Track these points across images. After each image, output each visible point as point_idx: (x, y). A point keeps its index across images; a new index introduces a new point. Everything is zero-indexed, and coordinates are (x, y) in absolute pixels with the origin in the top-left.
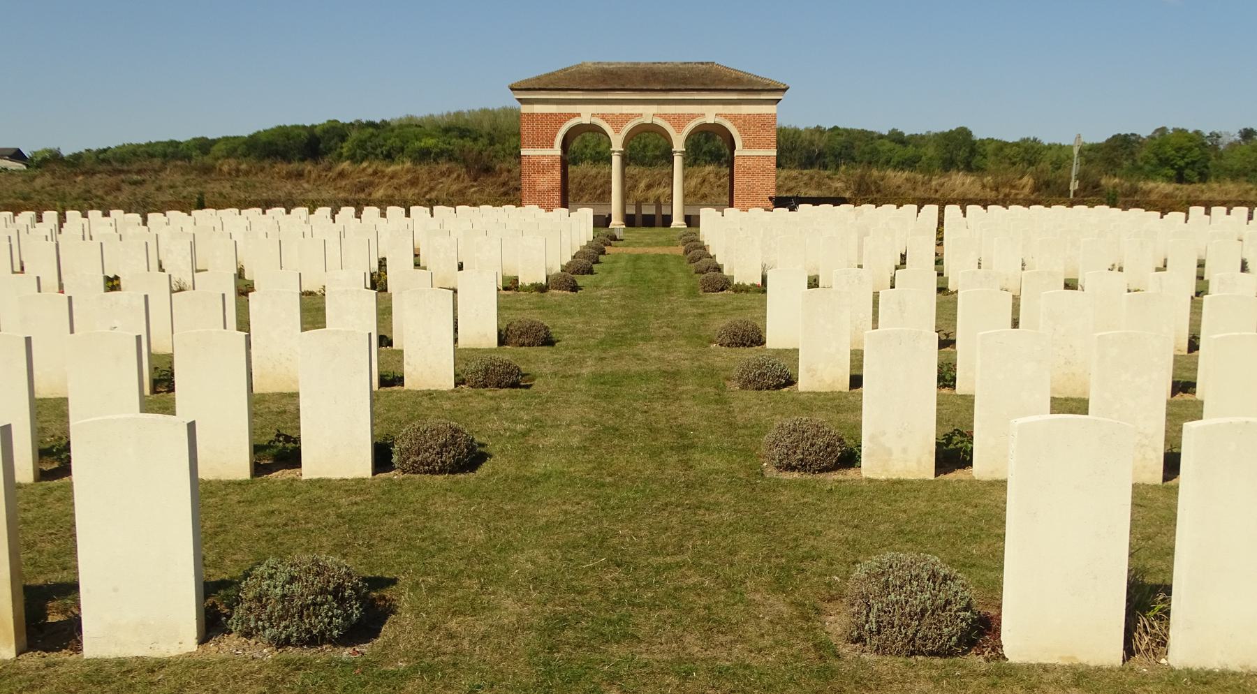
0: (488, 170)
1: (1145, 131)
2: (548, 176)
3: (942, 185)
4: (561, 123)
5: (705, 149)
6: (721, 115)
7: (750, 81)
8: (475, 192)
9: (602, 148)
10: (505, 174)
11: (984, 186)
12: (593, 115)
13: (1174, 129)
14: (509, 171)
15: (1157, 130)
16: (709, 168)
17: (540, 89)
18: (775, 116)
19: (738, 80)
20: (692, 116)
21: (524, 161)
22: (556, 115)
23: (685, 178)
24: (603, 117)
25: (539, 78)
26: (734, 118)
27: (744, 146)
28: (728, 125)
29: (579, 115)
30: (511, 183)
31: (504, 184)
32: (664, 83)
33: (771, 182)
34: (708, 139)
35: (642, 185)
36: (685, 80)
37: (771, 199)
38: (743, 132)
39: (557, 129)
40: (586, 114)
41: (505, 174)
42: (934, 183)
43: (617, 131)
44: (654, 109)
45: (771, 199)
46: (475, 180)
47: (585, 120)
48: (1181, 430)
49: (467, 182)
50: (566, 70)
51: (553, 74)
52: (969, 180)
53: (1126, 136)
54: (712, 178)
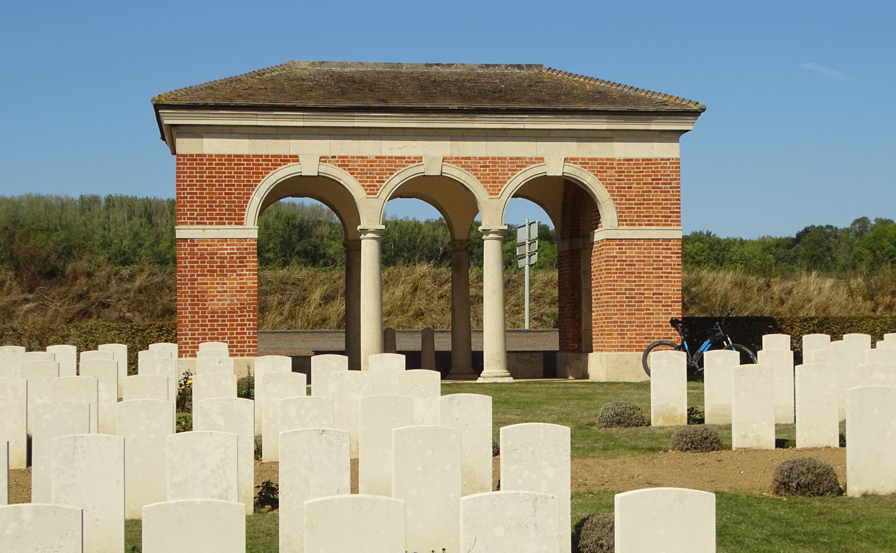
0: (52, 274)
1: (843, 221)
2: (233, 282)
3: (790, 292)
4: (259, 175)
5: (298, 248)
6: (574, 160)
7: (625, 98)
8: (31, 311)
9: (163, 246)
10: (83, 280)
11: (851, 293)
12: (323, 159)
13: (877, 220)
14: (89, 275)
15: (857, 221)
16: (423, 268)
17: (205, 107)
18: (677, 163)
19: (601, 95)
20: (519, 163)
21: (183, 252)
22: (248, 158)
23: (385, 284)
24: (344, 162)
25: (211, 88)
26: (600, 166)
27: (621, 220)
28: (589, 179)
29: (295, 158)
30: (94, 295)
31: (81, 297)
32: (463, 98)
33: (674, 290)
34: (301, 237)
35: (316, 296)
36: (497, 93)
37: (674, 322)
38: (617, 194)
39: (251, 187)
40: (310, 157)
41: (83, 280)
42: (776, 289)
43: (372, 190)
44: (444, 148)
45: (674, 322)
46: (31, 291)
47: (309, 167)
48: (137, 357)
49: (17, 295)
50: (260, 73)
51: (239, 80)
52: (829, 283)
53: (821, 228)
54: (428, 283)
